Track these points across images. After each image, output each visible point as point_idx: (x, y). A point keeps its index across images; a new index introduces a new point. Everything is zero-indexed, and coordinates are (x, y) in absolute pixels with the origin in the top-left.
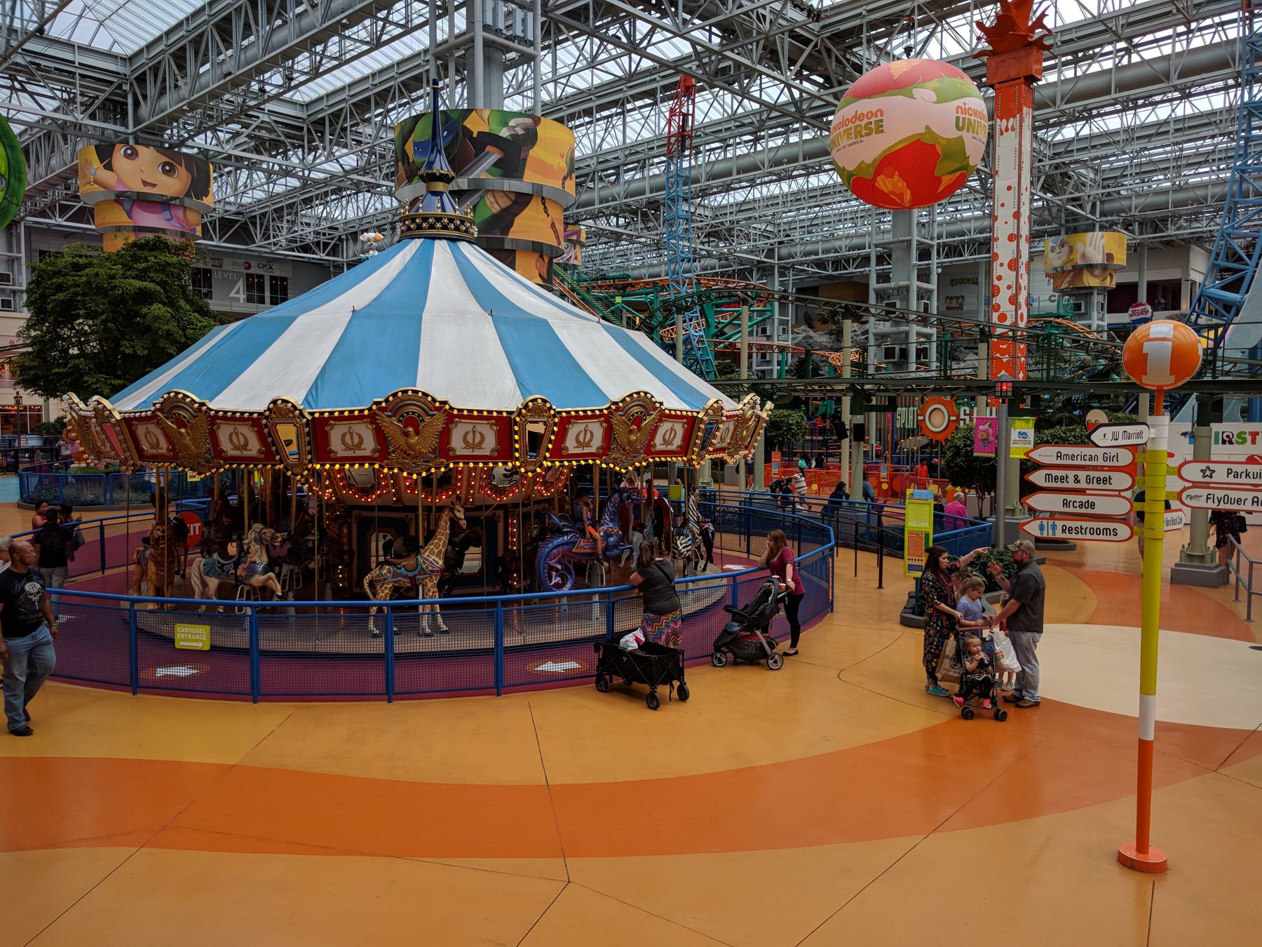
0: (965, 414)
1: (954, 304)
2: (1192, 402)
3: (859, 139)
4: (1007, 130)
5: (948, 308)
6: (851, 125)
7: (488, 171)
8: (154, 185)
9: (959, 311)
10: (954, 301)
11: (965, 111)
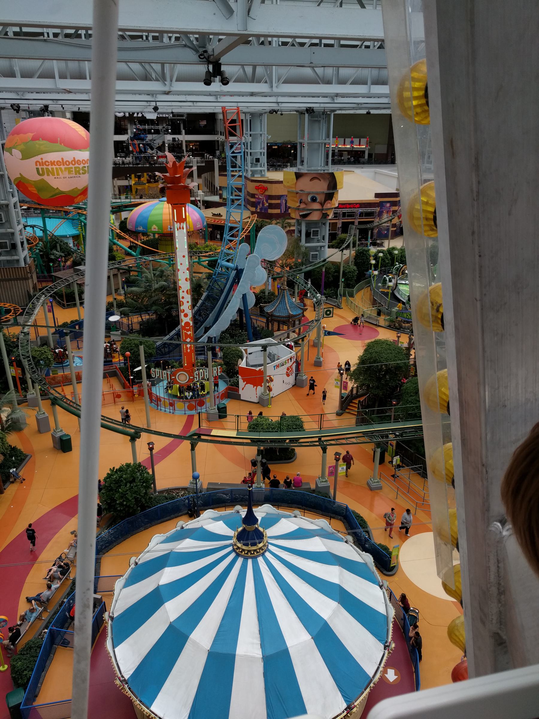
0: (196, 375)
3: (78, 175)
4: (180, 228)
6: (71, 166)
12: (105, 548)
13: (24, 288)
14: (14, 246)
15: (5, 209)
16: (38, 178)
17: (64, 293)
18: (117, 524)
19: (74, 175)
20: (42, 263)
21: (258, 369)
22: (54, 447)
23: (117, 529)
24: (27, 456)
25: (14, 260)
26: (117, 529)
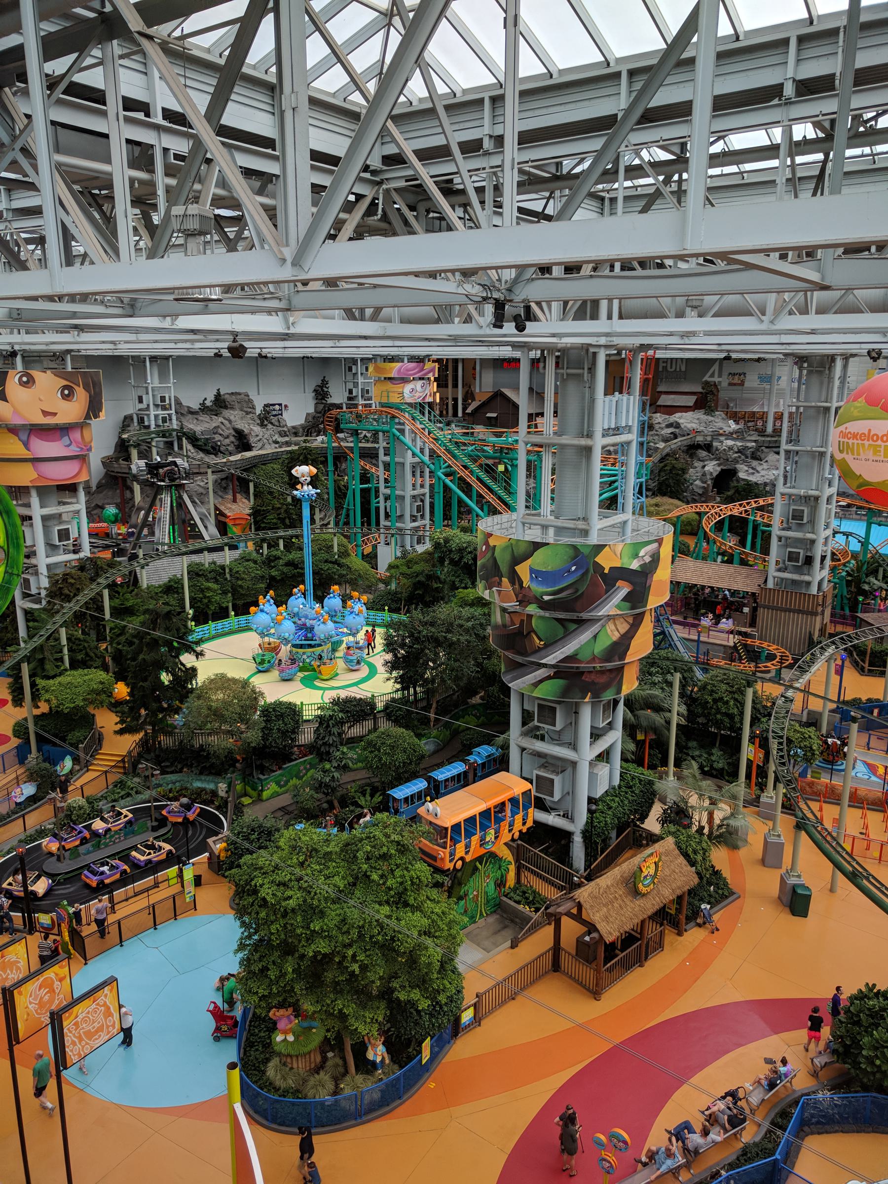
1: (736, 381)
5: (730, 384)
6: (879, 442)
7: (618, 607)
8: (55, 414)
9: (740, 388)
10: (736, 377)
12: (818, 1123)
13: (806, 629)
14: (809, 560)
15: (812, 503)
17: (869, 651)
18: (850, 1092)
20: (845, 593)
22: (779, 898)
23: (850, 1102)
24: (733, 893)
25: (802, 582)
26: (850, 1102)
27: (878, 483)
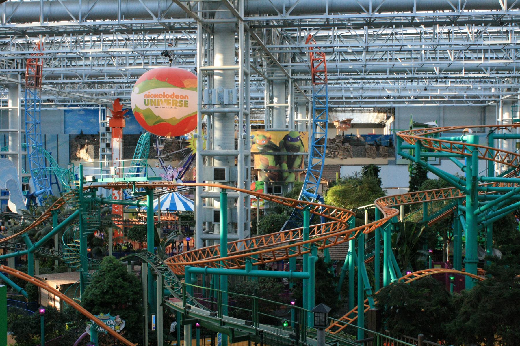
2: (480, 252)
3: (175, 107)
6: (170, 98)
11: (148, 96)
16: (145, 107)
19: (171, 106)
21: (372, 208)
27: (168, 120)
